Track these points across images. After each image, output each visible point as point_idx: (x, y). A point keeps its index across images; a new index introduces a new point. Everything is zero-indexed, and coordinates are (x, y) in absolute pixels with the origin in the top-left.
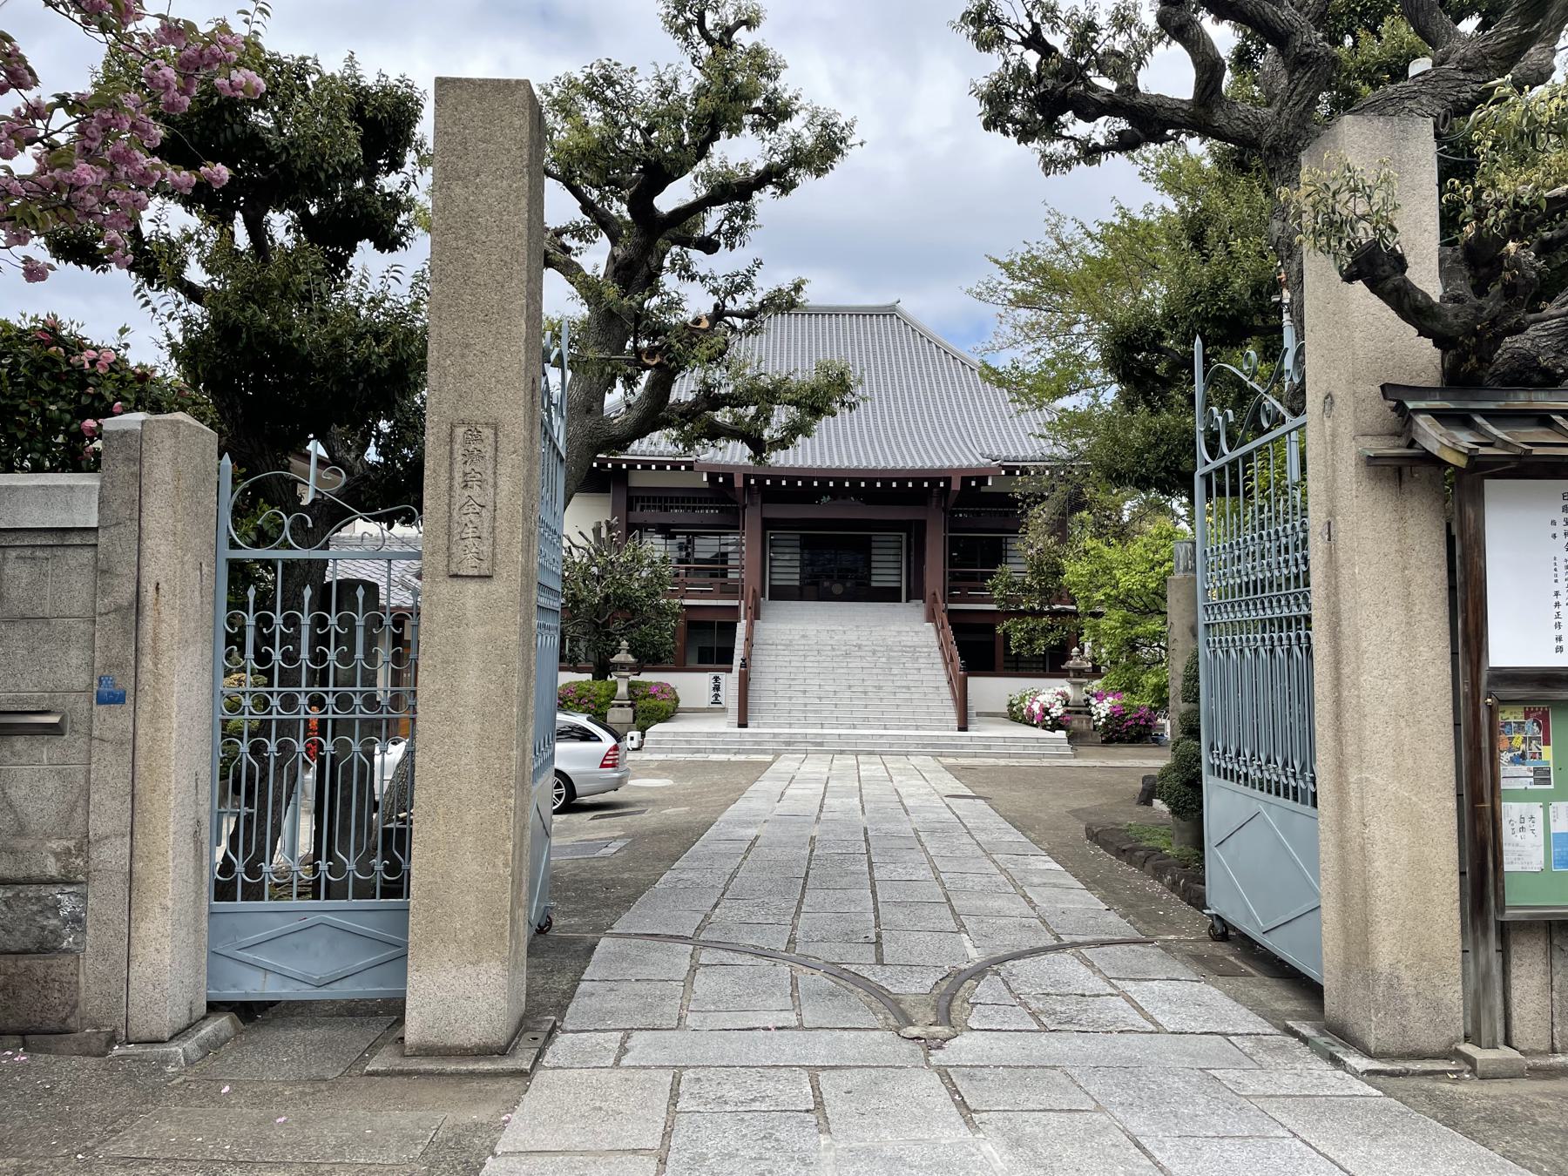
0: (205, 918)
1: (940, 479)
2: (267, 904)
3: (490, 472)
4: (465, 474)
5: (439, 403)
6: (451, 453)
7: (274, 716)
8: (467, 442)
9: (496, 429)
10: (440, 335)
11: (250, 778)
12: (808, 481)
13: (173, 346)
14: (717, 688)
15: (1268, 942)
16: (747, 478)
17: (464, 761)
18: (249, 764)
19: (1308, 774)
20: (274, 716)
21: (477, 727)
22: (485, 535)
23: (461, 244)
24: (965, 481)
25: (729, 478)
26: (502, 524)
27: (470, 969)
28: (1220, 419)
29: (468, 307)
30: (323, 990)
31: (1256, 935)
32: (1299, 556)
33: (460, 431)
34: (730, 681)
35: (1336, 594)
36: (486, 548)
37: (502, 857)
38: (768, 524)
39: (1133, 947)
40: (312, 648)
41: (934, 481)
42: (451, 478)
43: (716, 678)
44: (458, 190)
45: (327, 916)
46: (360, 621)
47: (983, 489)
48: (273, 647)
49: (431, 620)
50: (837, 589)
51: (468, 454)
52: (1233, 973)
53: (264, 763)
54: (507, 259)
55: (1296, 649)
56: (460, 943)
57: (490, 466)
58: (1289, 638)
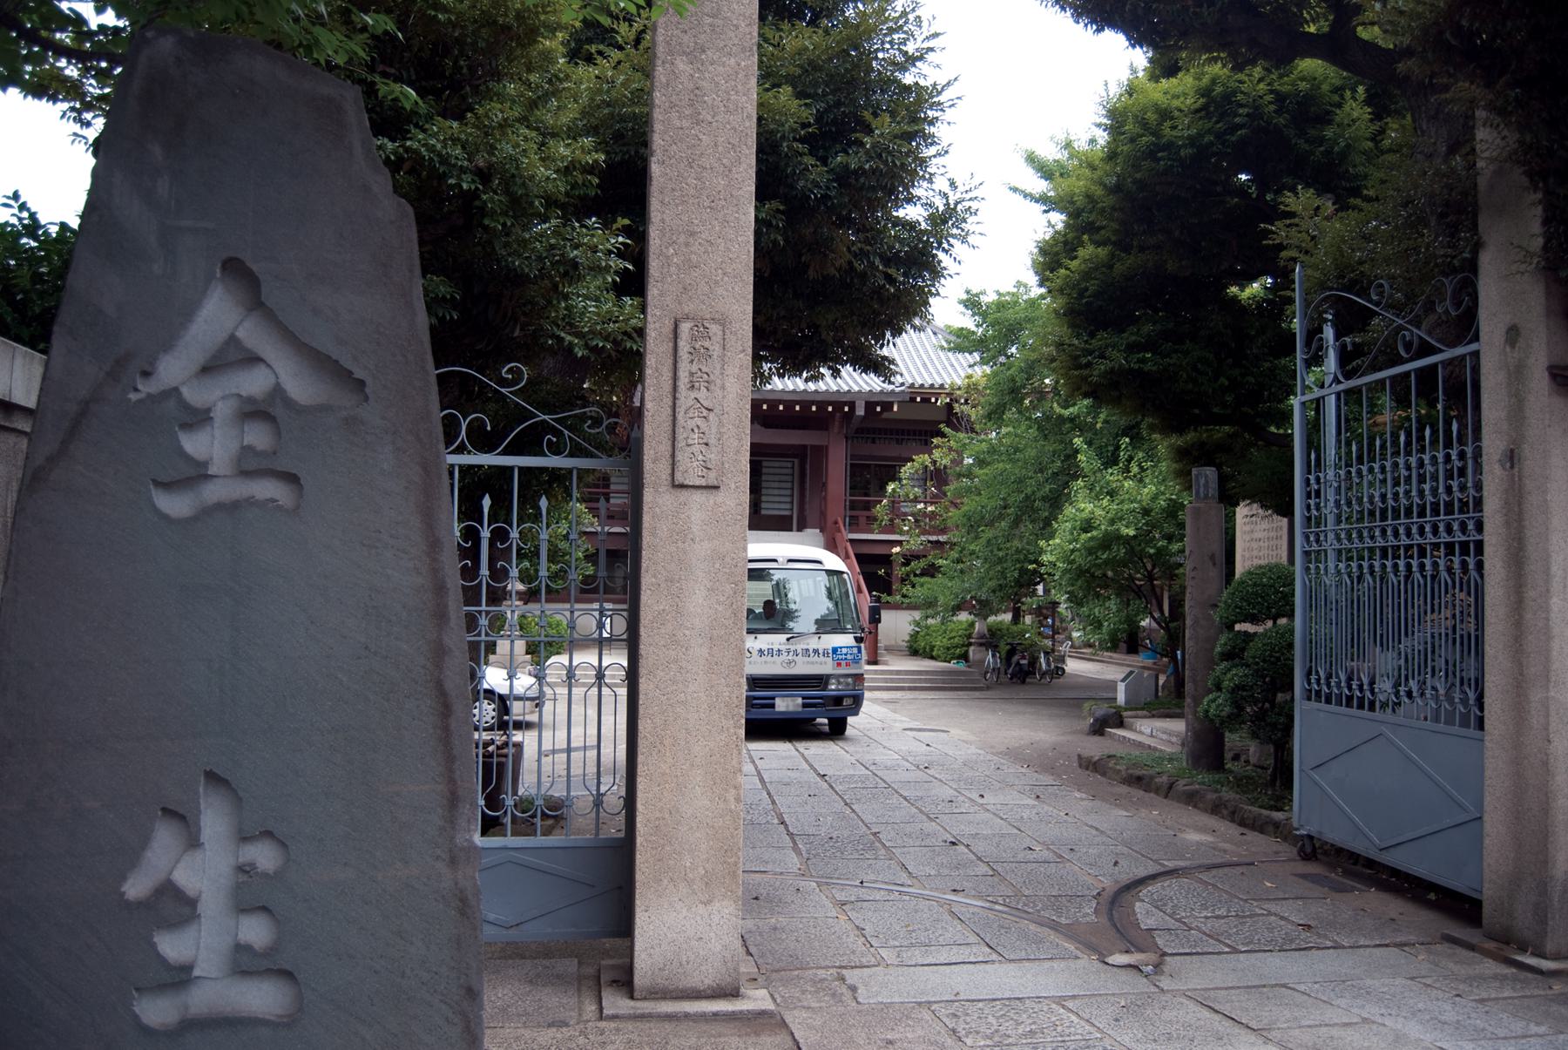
1: (845, 403)
3: (717, 372)
4: (692, 374)
5: (661, 295)
7: (483, 637)
8: (694, 339)
9: (723, 325)
10: (663, 221)
13: (1042, 199)
15: (1389, 859)
17: (692, 688)
20: (483, 637)
21: (705, 651)
22: (712, 441)
23: (685, 124)
24: (870, 406)
27: (701, 909)
29: (692, 192)
31: (1373, 854)
33: (685, 327)
37: (733, 791)
39: (1226, 870)
41: (838, 405)
42: (675, 378)
44: (681, 66)
46: (485, 534)
47: (885, 415)
48: (510, 563)
49: (654, 534)
52: (1353, 889)
54: (735, 141)
56: (690, 883)
57: (718, 366)
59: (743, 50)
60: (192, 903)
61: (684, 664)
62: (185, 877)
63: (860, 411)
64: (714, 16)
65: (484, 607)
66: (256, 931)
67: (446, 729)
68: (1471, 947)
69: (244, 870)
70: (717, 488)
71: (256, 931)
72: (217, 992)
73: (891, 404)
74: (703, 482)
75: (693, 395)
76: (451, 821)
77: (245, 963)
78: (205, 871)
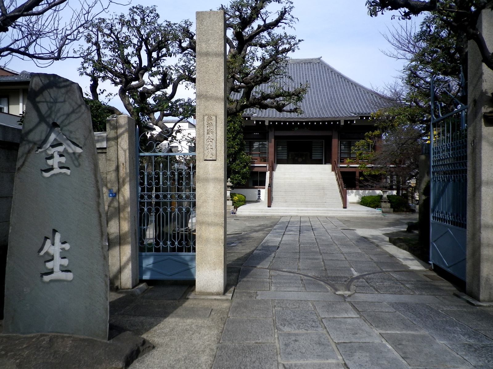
0: (138, 256)
1: (337, 121)
2: (161, 253)
4: (208, 130)
5: (200, 109)
6: (204, 124)
11: (178, 217)
12: (290, 122)
14: (259, 194)
16: (270, 122)
18: (178, 214)
19: (464, 218)
20: (146, 201)
24: (346, 121)
25: (263, 122)
26: (218, 144)
28: (439, 105)
30: (170, 277)
32: (464, 150)
33: (206, 117)
34: (264, 192)
35: (475, 162)
36: (214, 152)
38: (276, 138)
40: (148, 182)
43: (259, 191)
44: (203, 45)
45: (170, 256)
48: (152, 181)
50: (300, 160)
51: (208, 124)
53: (167, 214)
54: (218, 65)
55: (462, 180)
57: (215, 128)
58: (460, 176)
59: (220, 39)
60: (53, 256)
61: (208, 207)
62: (51, 251)
63: (342, 123)
64: (212, 30)
65: (146, 193)
66: (65, 262)
67: (100, 220)
68: (136, 237)
69: (63, 249)
70: (216, 160)
71: (65, 262)
72: (58, 275)
73: (353, 121)
74: (211, 159)
75: (208, 135)
76: (102, 239)
77: (65, 270)
78: (54, 248)
